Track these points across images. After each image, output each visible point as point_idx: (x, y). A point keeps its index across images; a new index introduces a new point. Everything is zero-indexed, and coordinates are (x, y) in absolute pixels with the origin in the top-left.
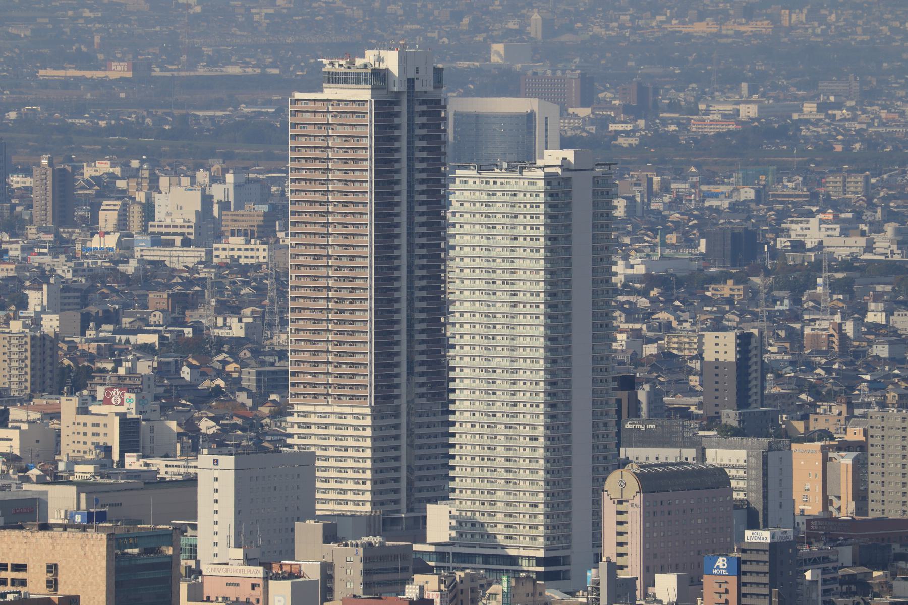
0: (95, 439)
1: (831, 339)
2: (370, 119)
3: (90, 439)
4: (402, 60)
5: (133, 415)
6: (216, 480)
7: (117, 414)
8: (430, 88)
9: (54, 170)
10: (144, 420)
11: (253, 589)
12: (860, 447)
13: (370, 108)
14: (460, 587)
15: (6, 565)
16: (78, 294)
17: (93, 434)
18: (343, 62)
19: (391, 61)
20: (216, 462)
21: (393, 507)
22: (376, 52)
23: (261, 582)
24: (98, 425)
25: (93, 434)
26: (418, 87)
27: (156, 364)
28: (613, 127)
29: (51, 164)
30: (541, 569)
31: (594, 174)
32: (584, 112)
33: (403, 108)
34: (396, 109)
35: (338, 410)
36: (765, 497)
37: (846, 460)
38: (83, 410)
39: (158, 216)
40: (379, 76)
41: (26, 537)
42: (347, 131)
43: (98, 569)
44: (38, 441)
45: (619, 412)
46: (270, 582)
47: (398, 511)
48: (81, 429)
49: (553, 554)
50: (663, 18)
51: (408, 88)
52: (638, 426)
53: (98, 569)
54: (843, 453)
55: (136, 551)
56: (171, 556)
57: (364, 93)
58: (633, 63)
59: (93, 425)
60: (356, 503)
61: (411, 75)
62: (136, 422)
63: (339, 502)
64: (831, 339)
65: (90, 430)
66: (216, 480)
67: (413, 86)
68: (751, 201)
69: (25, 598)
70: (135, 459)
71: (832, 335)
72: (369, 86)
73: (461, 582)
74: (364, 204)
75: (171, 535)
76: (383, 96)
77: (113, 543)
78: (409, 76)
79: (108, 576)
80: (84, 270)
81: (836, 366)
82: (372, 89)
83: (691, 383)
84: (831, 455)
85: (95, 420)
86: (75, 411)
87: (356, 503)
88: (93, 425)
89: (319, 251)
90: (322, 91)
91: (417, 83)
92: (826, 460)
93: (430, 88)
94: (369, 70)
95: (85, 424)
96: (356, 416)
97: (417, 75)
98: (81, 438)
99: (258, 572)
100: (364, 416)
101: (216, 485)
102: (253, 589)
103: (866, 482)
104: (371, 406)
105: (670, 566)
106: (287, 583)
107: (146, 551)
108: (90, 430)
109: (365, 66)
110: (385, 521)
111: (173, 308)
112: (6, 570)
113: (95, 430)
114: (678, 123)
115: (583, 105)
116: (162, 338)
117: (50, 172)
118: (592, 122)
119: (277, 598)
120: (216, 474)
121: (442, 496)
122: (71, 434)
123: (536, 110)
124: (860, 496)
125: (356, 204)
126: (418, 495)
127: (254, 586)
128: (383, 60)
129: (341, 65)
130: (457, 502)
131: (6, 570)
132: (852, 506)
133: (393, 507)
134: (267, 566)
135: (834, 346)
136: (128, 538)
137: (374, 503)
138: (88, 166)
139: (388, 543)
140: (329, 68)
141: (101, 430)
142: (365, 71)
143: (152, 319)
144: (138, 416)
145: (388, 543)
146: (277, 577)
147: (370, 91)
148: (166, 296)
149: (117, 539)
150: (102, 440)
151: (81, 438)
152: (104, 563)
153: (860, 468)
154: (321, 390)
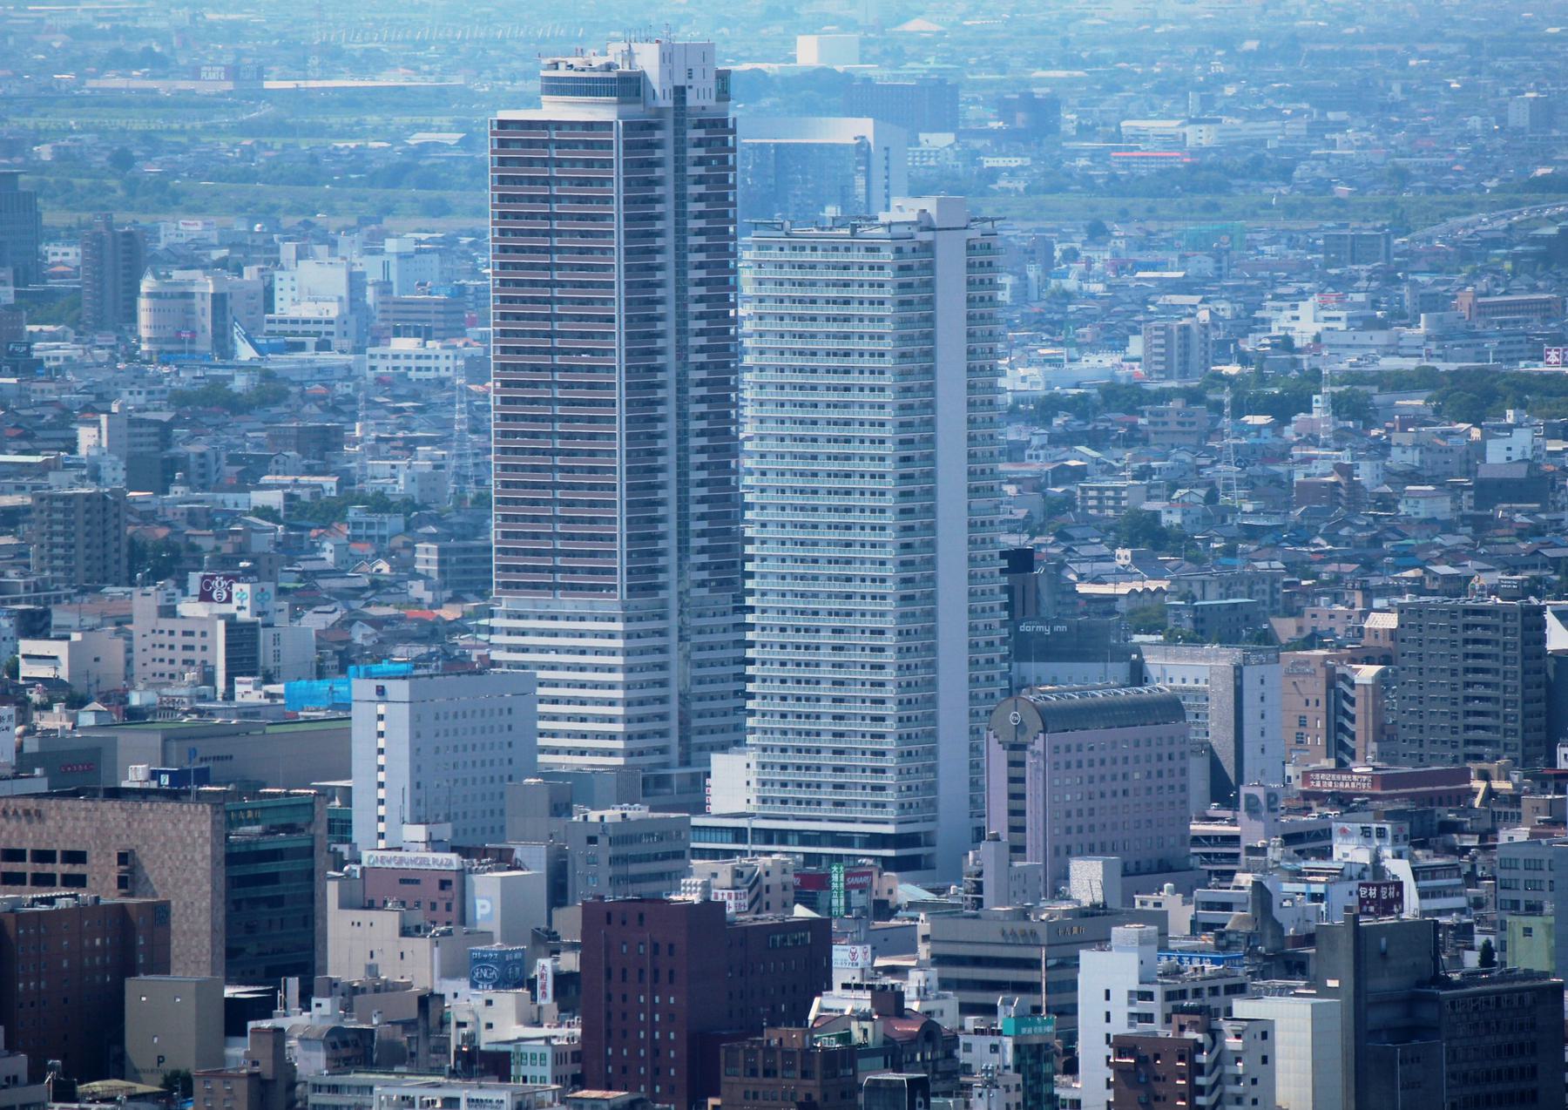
2: (617, 155)
6: (381, 717)
8: (710, 102)
10: (265, 626)
15: (53, 853)
16: (153, 430)
20: (381, 691)
21: (656, 759)
26: (692, 100)
31: (969, 234)
33: (666, 135)
34: (658, 135)
39: (278, 305)
43: (198, 857)
47: (665, 765)
51: (676, 101)
62: (251, 627)
65: (179, 640)
66: (381, 717)
67: (684, 99)
73: (767, 874)
75: (312, 805)
76: (636, 111)
78: (678, 83)
88: (185, 633)
90: (539, 106)
93: (710, 102)
97: (690, 82)
98: (166, 654)
108: (179, 640)
113: (188, 640)
120: (381, 709)
121: (732, 740)
122: (149, 647)
123: (871, 139)
133: (656, 759)
141: (196, 641)
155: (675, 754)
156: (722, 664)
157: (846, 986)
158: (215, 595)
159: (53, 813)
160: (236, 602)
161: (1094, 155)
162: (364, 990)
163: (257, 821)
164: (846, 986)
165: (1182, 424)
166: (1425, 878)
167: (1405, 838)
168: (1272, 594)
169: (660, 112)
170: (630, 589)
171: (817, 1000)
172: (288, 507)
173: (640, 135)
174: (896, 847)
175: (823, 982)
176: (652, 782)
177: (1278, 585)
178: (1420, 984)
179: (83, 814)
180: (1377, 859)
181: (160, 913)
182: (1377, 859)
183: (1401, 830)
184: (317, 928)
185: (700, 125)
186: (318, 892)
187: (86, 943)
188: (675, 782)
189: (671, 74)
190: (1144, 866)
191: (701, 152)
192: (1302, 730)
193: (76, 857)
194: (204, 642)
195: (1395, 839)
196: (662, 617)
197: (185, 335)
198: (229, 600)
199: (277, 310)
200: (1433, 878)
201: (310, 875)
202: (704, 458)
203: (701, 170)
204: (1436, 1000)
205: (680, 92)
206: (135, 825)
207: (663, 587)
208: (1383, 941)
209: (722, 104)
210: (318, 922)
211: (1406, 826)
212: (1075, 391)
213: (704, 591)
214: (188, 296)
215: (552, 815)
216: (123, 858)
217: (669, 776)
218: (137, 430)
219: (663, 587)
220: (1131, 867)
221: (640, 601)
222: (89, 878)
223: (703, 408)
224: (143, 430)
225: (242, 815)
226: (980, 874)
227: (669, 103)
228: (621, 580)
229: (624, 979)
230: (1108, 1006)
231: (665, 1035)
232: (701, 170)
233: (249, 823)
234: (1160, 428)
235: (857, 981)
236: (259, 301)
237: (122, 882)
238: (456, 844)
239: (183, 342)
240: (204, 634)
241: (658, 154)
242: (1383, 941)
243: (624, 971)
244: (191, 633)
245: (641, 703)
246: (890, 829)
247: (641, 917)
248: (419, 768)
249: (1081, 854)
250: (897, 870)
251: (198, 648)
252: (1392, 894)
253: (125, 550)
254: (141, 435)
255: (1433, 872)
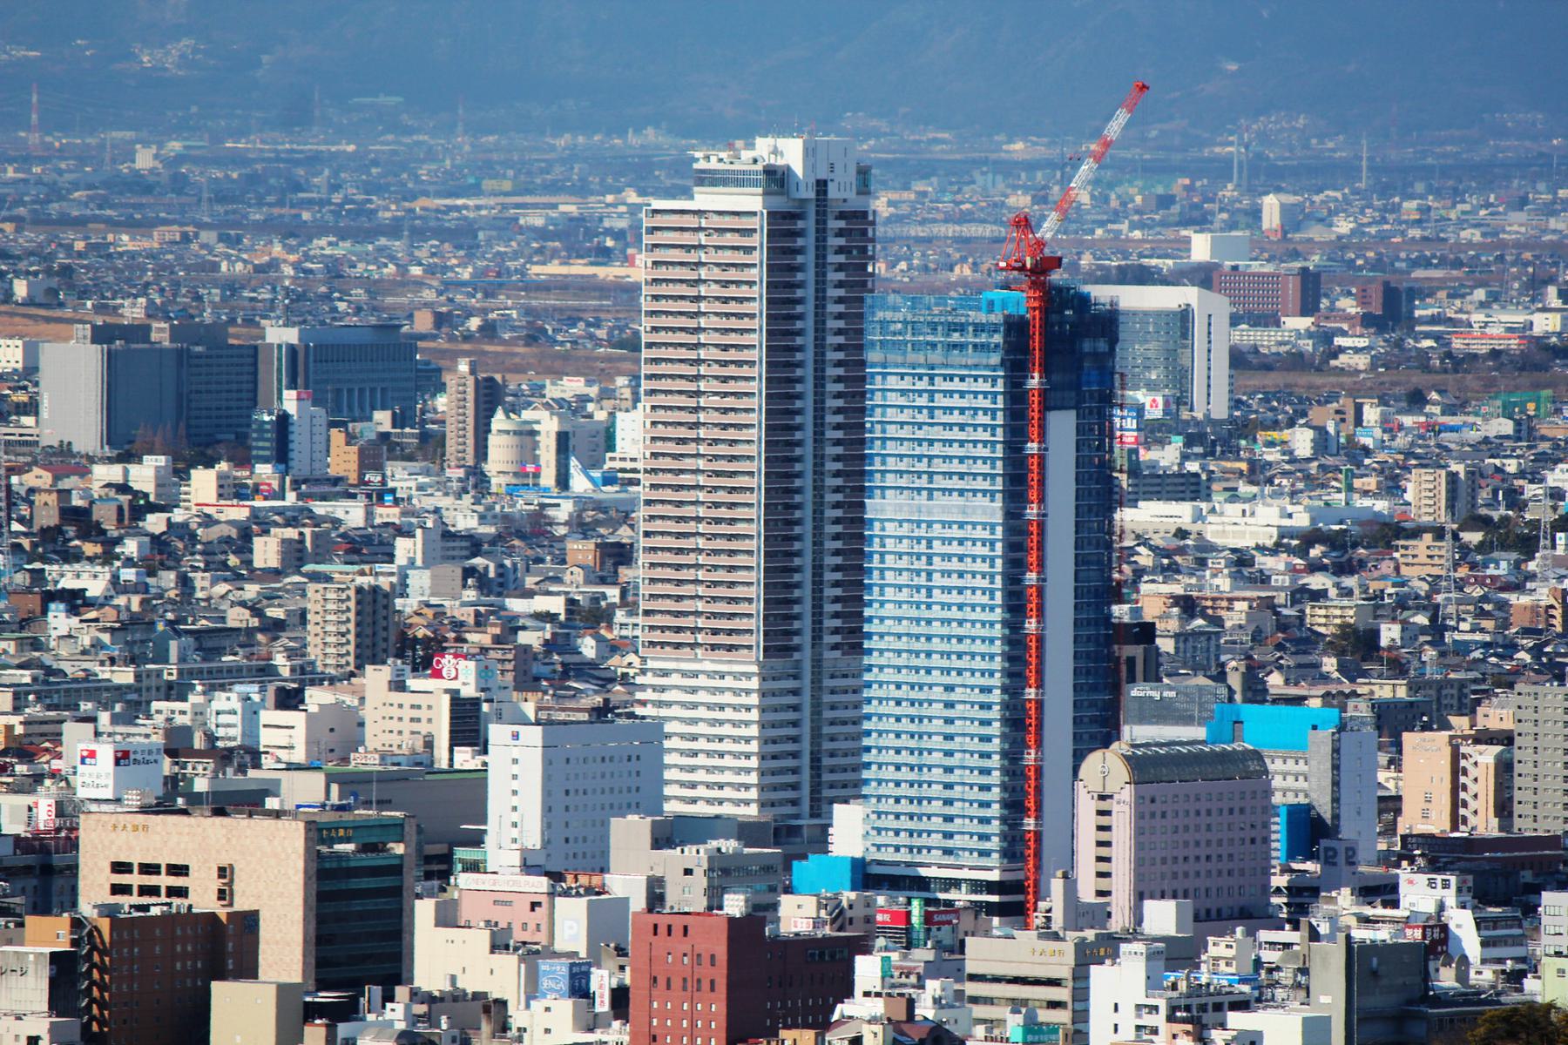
0: (415, 727)
1: (1553, 612)
2: (759, 240)
3: (407, 727)
4: (809, 152)
5: (469, 691)
6: (515, 761)
7: (447, 691)
8: (851, 195)
9: (477, 381)
10: (487, 701)
11: (533, 909)
12: (1507, 739)
13: (760, 223)
14: (849, 914)
15: (159, 866)
16: (464, 544)
17: (412, 720)
18: (723, 155)
19: (791, 153)
20: (516, 736)
21: (789, 810)
22: (770, 141)
23: (544, 899)
24: (419, 707)
25: (412, 720)
26: (833, 192)
27: (548, 636)
28: (1339, 341)
29: (473, 372)
30: (995, 898)
32: (1304, 323)
33: (809, 224)
34: (800, 224)
35: (708, 666)
36: (1336, 800)
37: (1487, 756)
38: (398, 686)
39: (619, 443)
40: (776, 178)
41: (190, 826)
42: (727, 257)
43: (291, 872)
44: (332, 730)
45: (404, 399)
46: (557, 899)
47: (797, 817)
48: (396, 712)
49: (1010, 876)
50: (1467, 207)
51: (818, 193)
52: (1150, 693)
53: (291, 872)
54: (1483, 747)
55: (350, 847)
56: (401, 857)
57: (752, 201)
58: (1404, 265)
59: (413, 707)
60: (737, 802)
61: (822, 174)
62: (475, 703)
63: (709, 801)
64: (1553, 612)
65: (408, 713)
66: (515, 761)
67: (825, 193)
68: (1507, 437)
69: (178, 913)
70: (468, 756)
71: (1552, 607)
72: (760, 190)
73: (851, 907)
74: (751, 363)
75: (402, 826)
76: (780, 203)
77: (313, 834)
79: (306, 885)
80: (495, 517)
81: (1548, 649)
82: (765, 194)
83: (1325, 669)
84: (1463, 750)
85: (416, 699)
86: (386, 686)
87: (737, 802)
88: (413, 707)
89: (683, 433)
90: (691, 197)
91: (830, 185)
92: (1456, 756)
93: (851, 195)
94: (759, 167)
95: (401, 706)
96: (737, 676)
97: (831, 176)
98: (395, 725)
99: (541, 884)
100: (748, 676)
101: (515, 769)
102: (533, 909)
103: (1511, 788)
104: (758, 663)
105: (1169, 892)
106: (583, 901)
107: (366, 848)
108: (408, 713)
109: (755, 161)
110: (777, 831)
111: (602, 563)
112: (159, 873)
113: (415, 713)
114: (1437, 337)
115: (1304, 312)
116: (571, 602)
117: (471, 382)
118: (1309, 335)
119: (568, 923)
120: (515, 753)
121: (851, 790)
122: (379, 719)
123: (1195, 305)
124: (1504, 808)
125: (739, 363)
126: (827, 793)
127: (534, 906)
128: (782, 154)
129: (721, 160)
130: (874, 800)
131: (159, 873)
132: (1495, 822)
133: (789, 810)
134: (556, 877)
135: (1554, 622)
136: (337, 829)
137: (763, 805)
138: (553, 384)
139: (747, 850)
140: (701, 165)
141: (423, 714)
142: (754, 167)
143: (567, 578)
144: (477, 695)
145: (747, 850)
146: (566, 893)
147: (760, 198)
148: (592, 547)
149: (320, 830)
150: (424, 728)
151: (395, 725)
152: (301, 864)
153: (1504, 768)
154: (686, 637)
155: (806, 806)
156: (774, 695)
157: (867, 994)
158: (444, 673)
159: (159, 828)
160: (461, 678)
161: (1437, 337)
162: (442, 999)
163: (348, 840)
164: (867, 994)
165: (1430, 557)
166: (1487, 928)
167: (1469, 890)
168: (1460, 699)
169: (803, 201)
170: (766, 649)
171: (839, 1007)
172: (569, 612)
173: (783, 226)
174: (999, 893)
175: (847, 991)
176: (784, 832)
177: (1466, 691)
178: (1410, 1002)
179: (186, 830)
180: (1441, 907)
181: (249, 921)
182: (1441, 907)
183: (1465, 882)
184: (405, 943)
185: (841, 216)
186: (406, 907)
187: (179, 948)
188: (805, 832)
189: (814, 167)
190: (1226, 912)
191: (841, 241)
192: (1428, 805)
193: (179, 870)
194: (430, 714)
195: (1459, 890)
196: (796, 677)
197: (530, 468)
198: (456, 678)
199: (618, 448)
200: (1495, 928)
201: (397, 892)
202: (839, 528)
203: (841, 259)
204: (1424, 1017)
205: (822, 186)
206: (234, 841)
207: (797, 648)
208: (1375, 961)
209: (862, 197)
210: (405, 936)
211: (1470, 878)
212: (1336, 527)
213: (837, 654)
214: (533, 433)
215: (653, 847)
216: (222, 872)
217: (800, 827)
218: (451, 544)
219: (797, 648)
220: (1203, 914)
221: (778, 663)
222: (108, 869)
223: (839, 482)
224: (457, 544)
225: (333, 834)
226: (1049, 911)
227: (812, 195)
228: (757, 640)
229: (668, 987)
230: (1116, 1018)
231: (662, 1024)
232: (841, 259)
233: (341, 841)
234: (1410, 560)
235: (878, 989)
236: (601, 439)
237: (222, 895)
238: (549, 868)
239: (527, 475)
240: (429, 707)
241: (800, 242)
242: (1375, 961)
243: (669, 980)
244: (419, 707)
245: (774, 757)
246: (994, 876)
247: (686, 928)
248: (550, 809)
249: (1152, 897)
250: (1000, 915)
251: (424, 721)
252: (1436, 936)
253: (392, 639)
254: (454, 548)
255: (1495, 922)
